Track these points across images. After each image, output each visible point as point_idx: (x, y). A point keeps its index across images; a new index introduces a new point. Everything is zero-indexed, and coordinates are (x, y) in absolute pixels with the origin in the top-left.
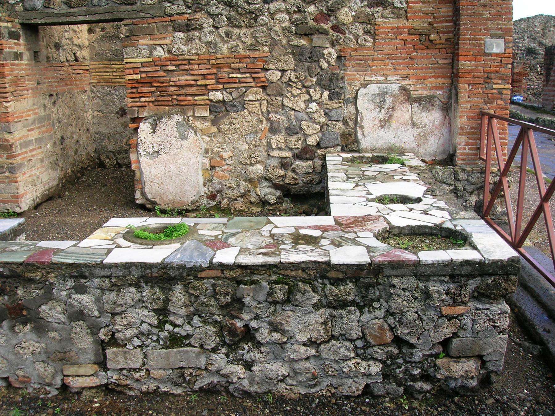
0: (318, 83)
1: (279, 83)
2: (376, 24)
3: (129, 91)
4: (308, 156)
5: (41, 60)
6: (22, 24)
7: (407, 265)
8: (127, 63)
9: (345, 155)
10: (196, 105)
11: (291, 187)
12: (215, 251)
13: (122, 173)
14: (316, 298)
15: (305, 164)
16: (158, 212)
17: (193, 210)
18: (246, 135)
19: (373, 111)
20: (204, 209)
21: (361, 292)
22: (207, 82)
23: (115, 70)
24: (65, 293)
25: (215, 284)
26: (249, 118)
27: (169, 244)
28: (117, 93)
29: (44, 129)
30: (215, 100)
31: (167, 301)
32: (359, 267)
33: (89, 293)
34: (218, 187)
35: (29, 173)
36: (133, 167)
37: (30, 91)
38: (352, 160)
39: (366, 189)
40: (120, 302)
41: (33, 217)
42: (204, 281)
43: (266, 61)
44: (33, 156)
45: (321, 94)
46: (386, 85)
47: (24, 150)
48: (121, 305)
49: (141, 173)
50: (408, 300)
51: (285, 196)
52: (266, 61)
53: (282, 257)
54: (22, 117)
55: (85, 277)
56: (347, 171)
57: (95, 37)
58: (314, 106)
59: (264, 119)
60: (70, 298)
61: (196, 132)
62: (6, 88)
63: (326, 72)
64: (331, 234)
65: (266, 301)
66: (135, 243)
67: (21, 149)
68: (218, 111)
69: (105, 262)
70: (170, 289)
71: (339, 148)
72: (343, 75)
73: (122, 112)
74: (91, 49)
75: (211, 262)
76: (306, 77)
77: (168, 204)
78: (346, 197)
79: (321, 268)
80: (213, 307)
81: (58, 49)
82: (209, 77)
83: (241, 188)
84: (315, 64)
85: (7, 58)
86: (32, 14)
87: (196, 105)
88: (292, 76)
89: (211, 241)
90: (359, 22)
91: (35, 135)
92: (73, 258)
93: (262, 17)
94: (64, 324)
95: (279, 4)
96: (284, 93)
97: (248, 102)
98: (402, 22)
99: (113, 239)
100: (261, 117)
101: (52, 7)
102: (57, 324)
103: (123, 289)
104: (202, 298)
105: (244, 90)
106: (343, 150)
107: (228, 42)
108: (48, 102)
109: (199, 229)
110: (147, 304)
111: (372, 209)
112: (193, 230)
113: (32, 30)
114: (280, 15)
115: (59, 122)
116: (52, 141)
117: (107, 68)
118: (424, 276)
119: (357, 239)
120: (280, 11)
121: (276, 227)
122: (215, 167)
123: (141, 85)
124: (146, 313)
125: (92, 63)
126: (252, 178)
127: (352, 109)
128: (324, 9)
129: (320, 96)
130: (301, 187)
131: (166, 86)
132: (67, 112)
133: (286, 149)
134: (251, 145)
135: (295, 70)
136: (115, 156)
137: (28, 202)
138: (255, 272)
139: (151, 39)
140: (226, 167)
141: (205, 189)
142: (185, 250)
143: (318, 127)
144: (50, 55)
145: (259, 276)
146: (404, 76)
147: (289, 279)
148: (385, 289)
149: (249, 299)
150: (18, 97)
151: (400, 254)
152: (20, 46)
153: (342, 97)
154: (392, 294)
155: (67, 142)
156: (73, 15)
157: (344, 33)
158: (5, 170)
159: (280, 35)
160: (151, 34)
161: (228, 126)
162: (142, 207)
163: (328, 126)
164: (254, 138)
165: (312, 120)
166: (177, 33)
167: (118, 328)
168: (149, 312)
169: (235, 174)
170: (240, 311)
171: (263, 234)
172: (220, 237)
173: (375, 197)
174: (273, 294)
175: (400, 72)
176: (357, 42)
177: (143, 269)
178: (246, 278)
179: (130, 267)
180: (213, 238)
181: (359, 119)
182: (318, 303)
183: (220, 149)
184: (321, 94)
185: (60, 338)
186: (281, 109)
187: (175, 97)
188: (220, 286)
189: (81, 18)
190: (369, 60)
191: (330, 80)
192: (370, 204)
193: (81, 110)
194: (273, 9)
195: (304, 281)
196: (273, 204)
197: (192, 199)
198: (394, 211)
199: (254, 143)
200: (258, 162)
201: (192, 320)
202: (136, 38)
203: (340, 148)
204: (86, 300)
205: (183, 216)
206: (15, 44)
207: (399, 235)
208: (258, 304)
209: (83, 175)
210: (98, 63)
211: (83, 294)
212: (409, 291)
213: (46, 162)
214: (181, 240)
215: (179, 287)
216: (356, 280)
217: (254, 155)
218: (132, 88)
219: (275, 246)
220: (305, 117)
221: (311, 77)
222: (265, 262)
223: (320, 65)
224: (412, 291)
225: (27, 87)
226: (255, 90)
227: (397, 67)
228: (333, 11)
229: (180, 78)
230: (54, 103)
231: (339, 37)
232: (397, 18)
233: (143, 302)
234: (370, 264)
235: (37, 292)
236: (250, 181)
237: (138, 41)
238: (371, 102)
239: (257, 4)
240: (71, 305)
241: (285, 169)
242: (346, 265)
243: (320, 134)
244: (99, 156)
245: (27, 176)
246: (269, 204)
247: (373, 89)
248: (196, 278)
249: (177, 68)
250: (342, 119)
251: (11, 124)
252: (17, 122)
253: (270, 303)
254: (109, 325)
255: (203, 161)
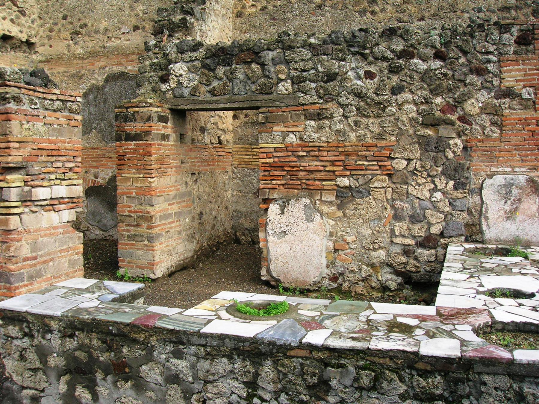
0: (444, 173)
1: (405, 171)
2: (503, 116)
3: (262, 174)
4: (430, 244)
5: (186, 141)
6: (171, 110)
7: (500, 363)
8: (261, 148)
9: (467, 246)
10: (324, 189)
11: (412, 274)
12: (307, 331)
13: (255, 249)
14: (402, 388)
15: (427, 252)
16: (281, 290)
17: (314, 290)
18: (371, 221)
19: (498, 202)
20: (325, 290)
21: (450, 386)
22: (335, 168)
23: (255, 153)
24: (164, 356)
25: (303, 364)
26: (374, 204)
27: (266, 320)
28: (256, 175)
29: (184, 204)
30: (342, 185)
31: (257, 375)
32: (449, 361)
33: (186, 359)
34: (341, 270)
35: (166, 244)
36: (261, 245)
37: (174, 169)
38: (474, 252)
39: (479, 281)
40: (213, 371)
41: (165, 284)
42: (293, 359)
43: (392, 150)
44: (171, 228)
45: (446, 184)
46: (513, 176)
47: (163, 222)
48: (214, 374)
49: (268, 251)
50: (500, 400)
51: (406, 283)
52: (392, 150)
53: (372, 343)
54: (164, 192)
55: (183, 344)
56: (465, 262)
57: (239, 122)
58: (438, 195)
59: (389, 206)
60: (168, 361)
61: (322, 216)
62: (151, 165)
63: (452, 162)
64: (429, 325)
65: (352, 386)
66: (235, 316)
67: (160, 221)
68: (344, 196)
69: (202, 331)
70: (261, 364)
71: (463, 238)
72: (468, 165)
73: (257, 193)
74: (234, 133)
75: (300, 342)
76: (431, 166)
77: (291, 283)
78: (456, 290)
79: (409, 358)
80: (300, 386)
81: (203, 133)
82: (337, 163)
83: (363, 272)
84: (441, 154)
85: (155, 139)
86: (181, 101)
87: (324, 189)
88: (417, 165)
89: (307, 322)
90: (485, 114)
91: (175, 209)
92: (174, 324)
93: (390, 108)
94: (161, 385)
95: (406, 95)
96: (409, 181)
98: (530, 114)
99: (216, 311)
100: (385, 204)
101: (198, 94)
102: (154, 385)
103: (217, 359)
104: (290, 376)
105: (370, 177)
106: (467, 241)
107: (356, 131)
108: (190, 180)
109: (299, 309)
110: (237, 376)
111: (478, 303)
112: (292, 309)
113: (180, 115)
114: (408, 106)
115: (200, 199)
116: (191, 216)
117: (248, 151)
118: (518, 376)
119: (453, 332)
120: (407, 102)
121: (375, 313)
122: (338, 250)
123: (273, 168)
124: (236, 384)
125: (234, 146)
126: (374, 263)
127: (477, 199)
128: (451, 100)
129: (445, 185)
130: (422, 275)
131: (297, 171)
132: (207, 190)
133: (409, 236)
134: (374, 231)
135: (420, 160)
136: (250, 233)
137: (162, 269)
138: (343, 356)
139: (285, 127)
140: (349, 251)
141: (327, 271)
142: (279, 327)
143: (442, 216)
144: (195, 138)
145: (346, 360)
146: (531, 167)
147: (377, 366)
148: (475, 386)
149: (335, 382)
150: (162, 174)
151: (495, 351)
152: (168, 129)
153: (468, 187)
154: (483, 392)
155: (205, 217)
156: (216, 102)
157: (470, 124)
158: (144, 239)
159: (407, 125)
160: (285, 122)
161: (354, 212)
162: (267, 283)
163: (452, 215)
164: (378, 224)
165: (436, 208)
166: (309, 121)
167: (210, 395)
168: (239, 384)
169: (358, 258)
170: (326, 393)
171: (360, 318)
172: (317, 318)
173: (486, 290)
174: (359, 379)
175: (528, 163)
176: (484, 133)
177: (236, 342)
178: (334, 361)
179: (225, 339)
180: (310, 319)
181: (484, 210)
182: (404, 393)
183: (344, 233)
184: (446, 184)
185: (155, 398)
186: (405, 197)
187: (304, 181)
188: (308, 366)
189: (222, 106)
190: (495, 150)
191: (456, 170)
192: (478, 296)
193: (222, 189)
194: (400, 100)
195: (391, 370)
196: (393, 290)
197: (314, 280)
198: (502, 305)
199: (377, 229)
200: (381, 248)
201: (279, 396)
202: (271, 125)
203: (463, 238)
204: (182, 365)
205: (304, 295)
206: (163, 126)
207: (502, 330)
208: (344, 388)
209: (218, 249)
210: (240, 146)
211: (180, 359)
212: (501, 391)
213: (183, 234)
214: (278, 318)
215: (269, 363)
216: (445, 374)
217: (377, 241)
218: (265, 171)
219: (368, 332)
220: (430, 205)
221: (437, 167)
222: (353, 347)
223: (446, 154)
224: (504, 391)
225: (171, 165)
226: (381, 177)
227: (524, 158)
228: (460, 103)
229: (310, 164)
230: (196, 181)
231: (465, 128)
232: (525, 109)
233: (235, 373)
234: (460, 359)
235: (140, 353)
236: (372, 265)
237: (273, 127)
238: (497, 193)
239: (385, 95)
240: (169, 369)
241: (407, 256)
242: (435, 357)
243: (444, 224)
244: (235, 233)
245: (164, 245)
246: (390, 290)
247: (499, 180)
248: (286, 356)
249: (308, 154)
250: (466, 209)
251: (154, 198)
252: (159, 196)
253: (356, 388)
254: (201, 391)
255: (328, 244)
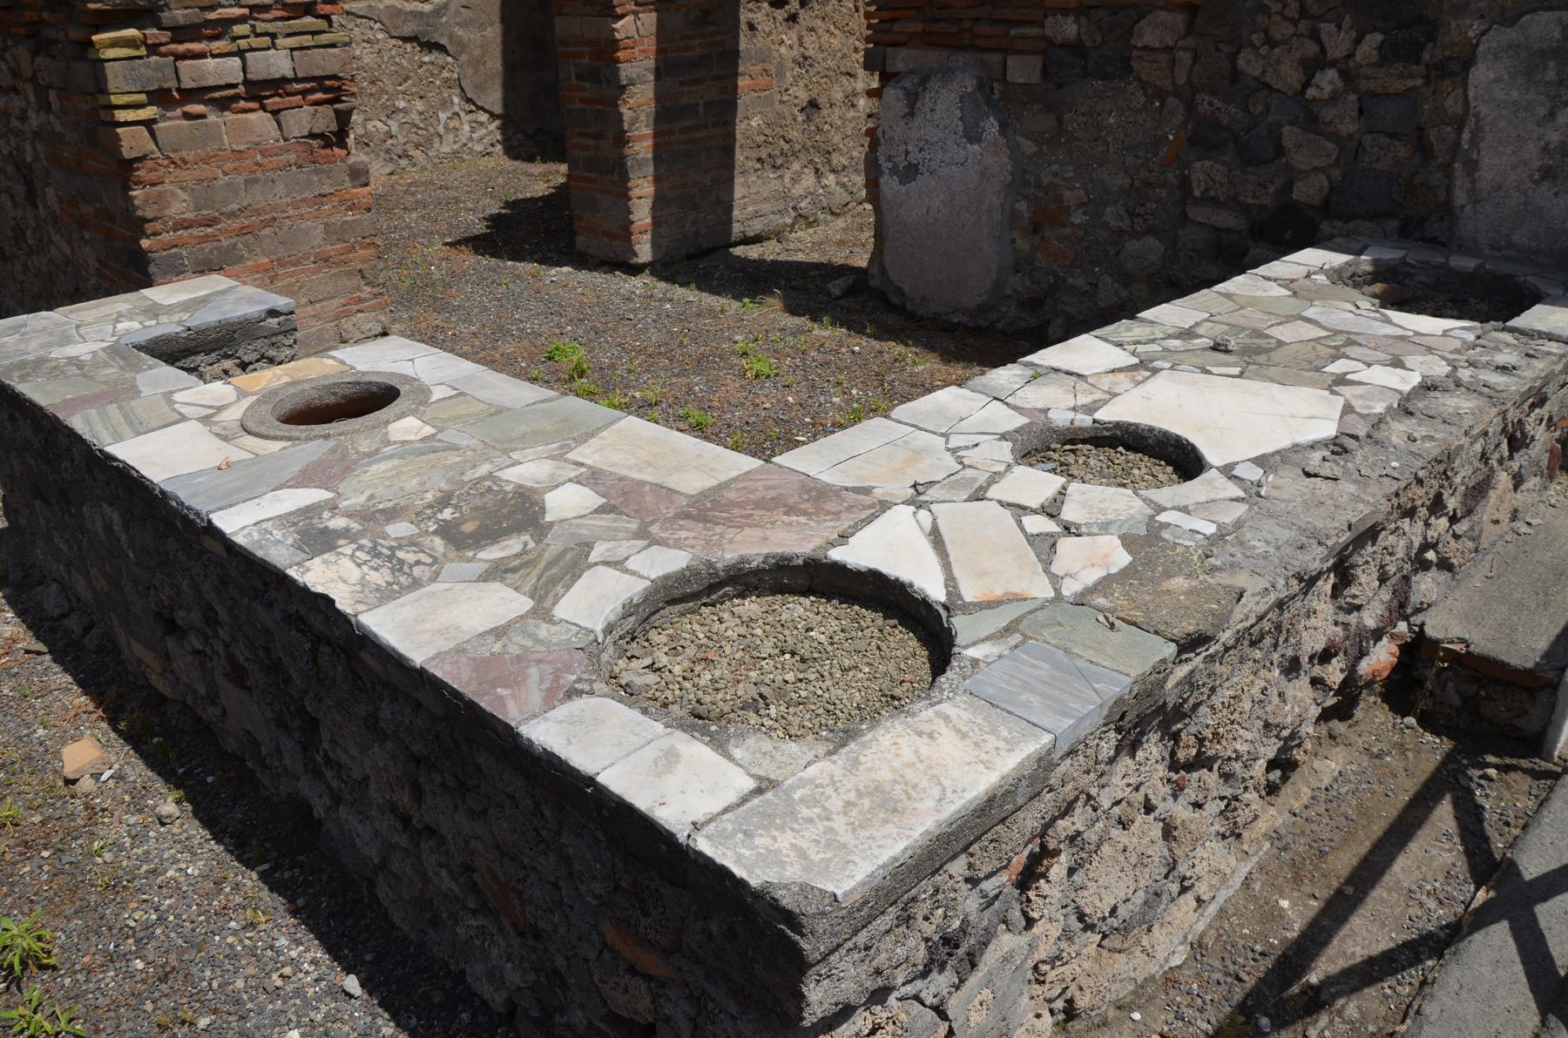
30: (1059, 39)
97: (1140, 53)
